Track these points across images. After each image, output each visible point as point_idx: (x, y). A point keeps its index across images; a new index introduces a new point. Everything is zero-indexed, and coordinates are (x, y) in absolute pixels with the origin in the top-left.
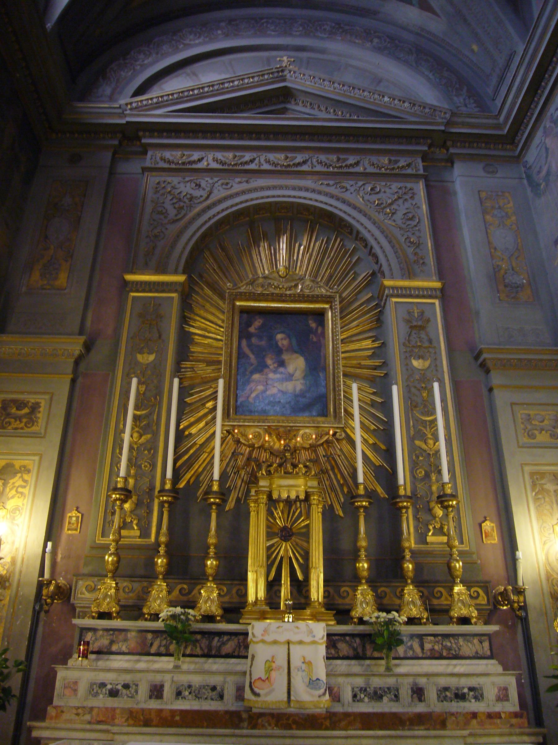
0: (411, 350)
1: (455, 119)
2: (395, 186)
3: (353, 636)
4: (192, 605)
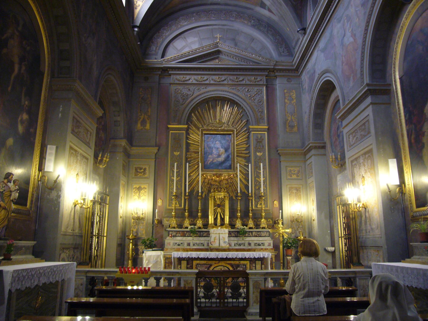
0: (257, 149)
1: (277, 64)
2: (256, 88)
3: (235, 232)
4: (195, 225)
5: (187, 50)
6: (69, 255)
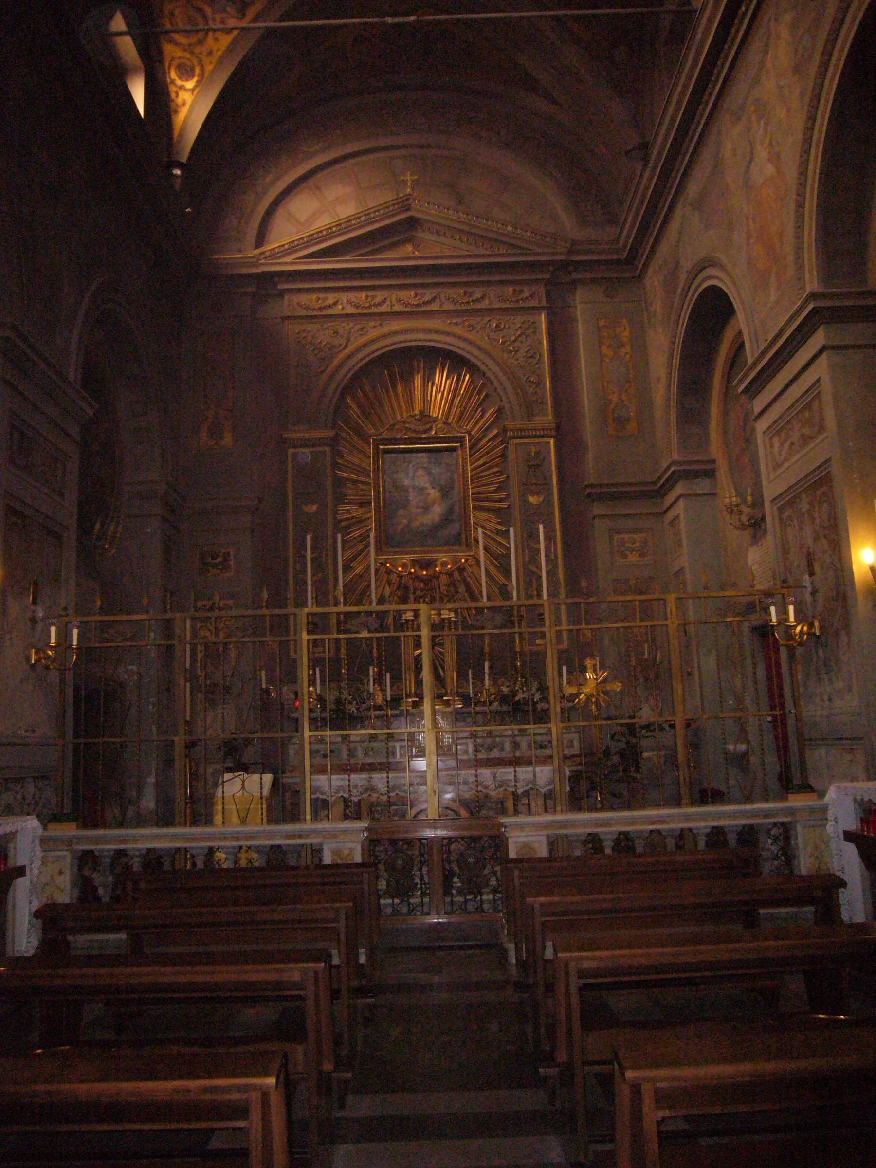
2: (519, 320)
5: (324, 221)
6: (24, 798)
